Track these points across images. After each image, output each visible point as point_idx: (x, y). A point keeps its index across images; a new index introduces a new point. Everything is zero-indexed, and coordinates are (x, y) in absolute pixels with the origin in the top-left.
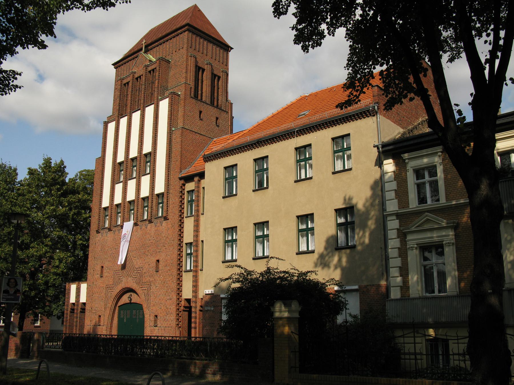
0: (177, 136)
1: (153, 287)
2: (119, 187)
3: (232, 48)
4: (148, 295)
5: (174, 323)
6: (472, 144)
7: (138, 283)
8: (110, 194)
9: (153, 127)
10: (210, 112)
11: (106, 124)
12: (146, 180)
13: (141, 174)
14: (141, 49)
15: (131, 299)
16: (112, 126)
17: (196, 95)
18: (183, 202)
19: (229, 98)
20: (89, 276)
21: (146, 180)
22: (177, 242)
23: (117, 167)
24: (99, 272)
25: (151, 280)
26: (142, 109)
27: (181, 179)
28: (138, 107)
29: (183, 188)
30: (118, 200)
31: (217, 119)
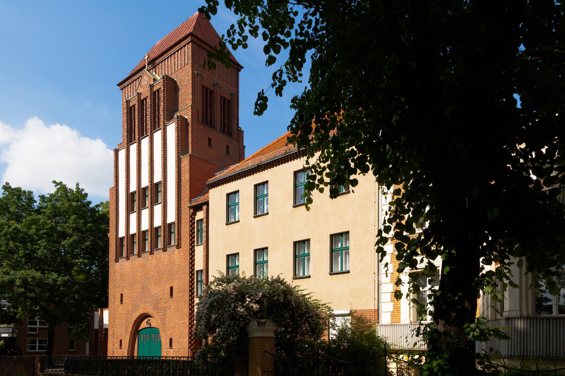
0: (186, 161)
1: (168, 312)
2: (133, 217)
3: (242, 68)
4: (163, 320)
5: (187, 346)
6: (508, 165)
7: (154, 309)
8: (125, 224)
9: (162, 154)
10: (220, 139)
11: (117, 152)
12: (158, 209)
13: (155, 202)
14: (144, 67)
15: (150, 324)
16: (122, 154)
17: (203, 122)
18: (193, 236)
19: (240, 126)
20: (110, 304)
21: (158, 209)
22: (188, 270)
23: (130, 197)
24: (119, 299)
25: (166, 305)
26: (149, 135)
27: (190, 208)
28: (146, 134)
29: (193, 217)
30: (133, 230)
31: (227, 147)
